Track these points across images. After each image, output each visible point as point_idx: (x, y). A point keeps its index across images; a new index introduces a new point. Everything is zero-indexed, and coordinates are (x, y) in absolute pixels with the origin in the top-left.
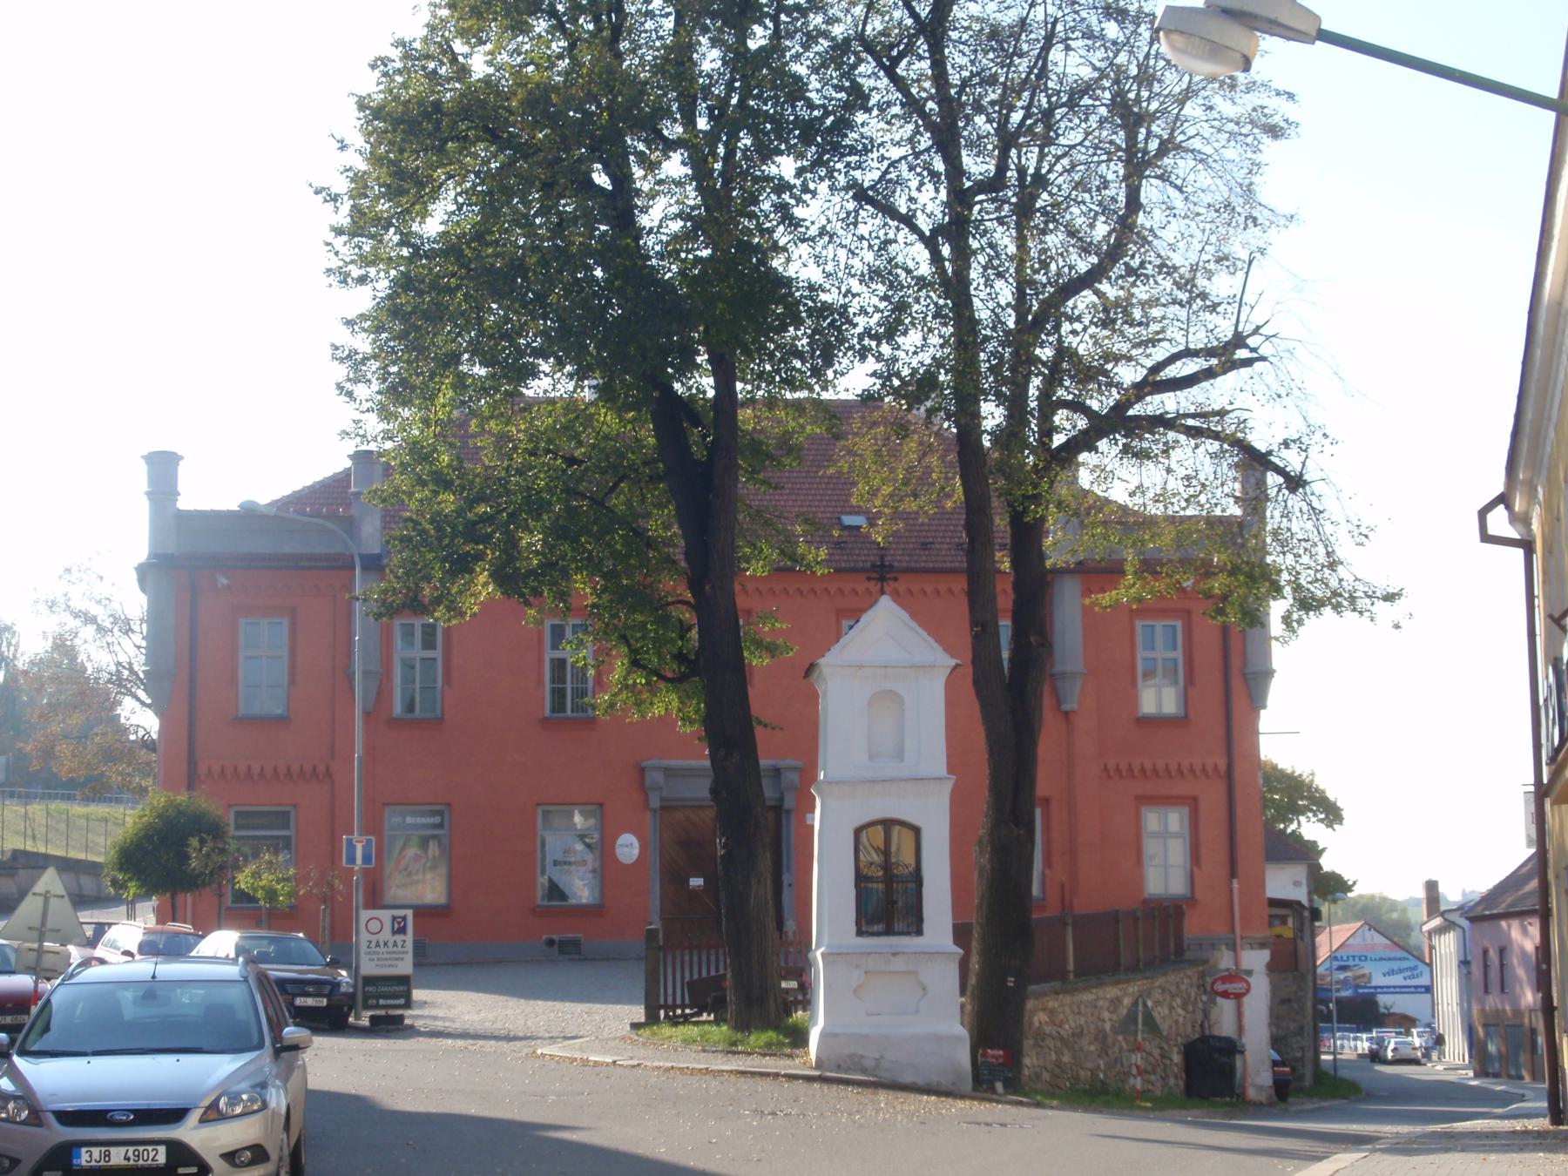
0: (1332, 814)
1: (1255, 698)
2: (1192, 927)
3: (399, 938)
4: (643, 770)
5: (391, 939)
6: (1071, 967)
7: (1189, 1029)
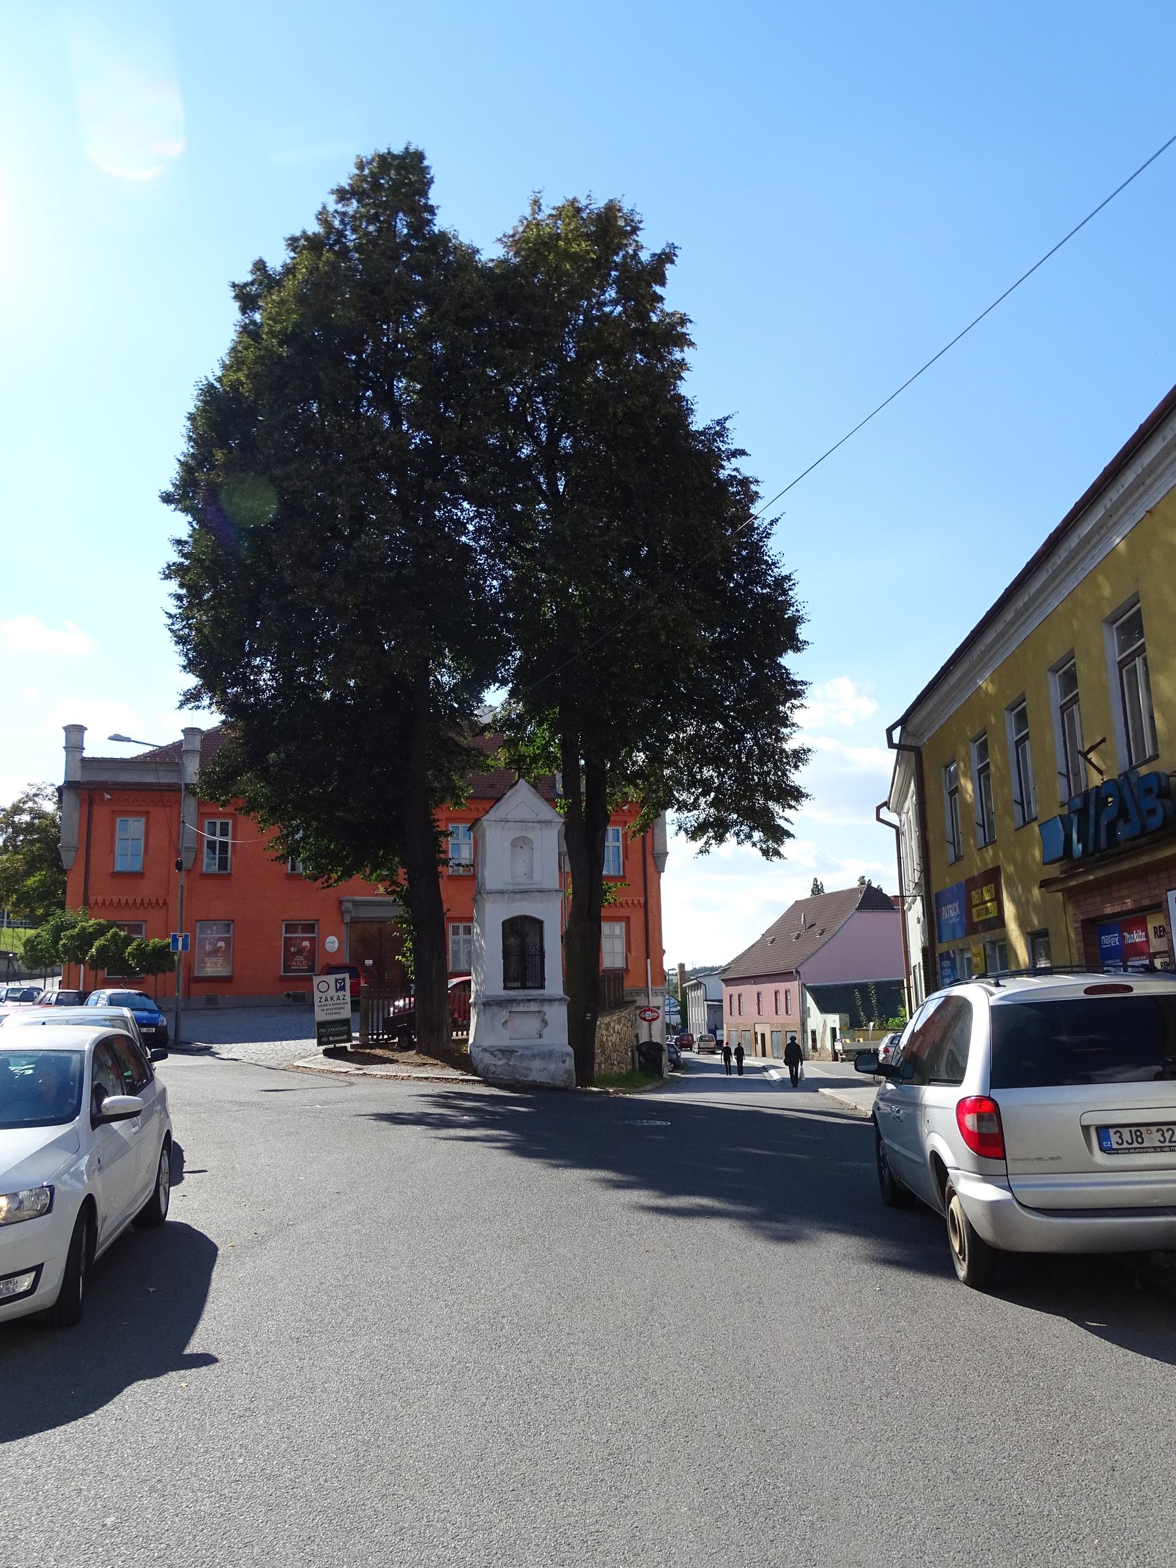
1: (659, 869)
2: (628, 984)
3: (341, 993)
4: (341, 902)
5: (335, 995)
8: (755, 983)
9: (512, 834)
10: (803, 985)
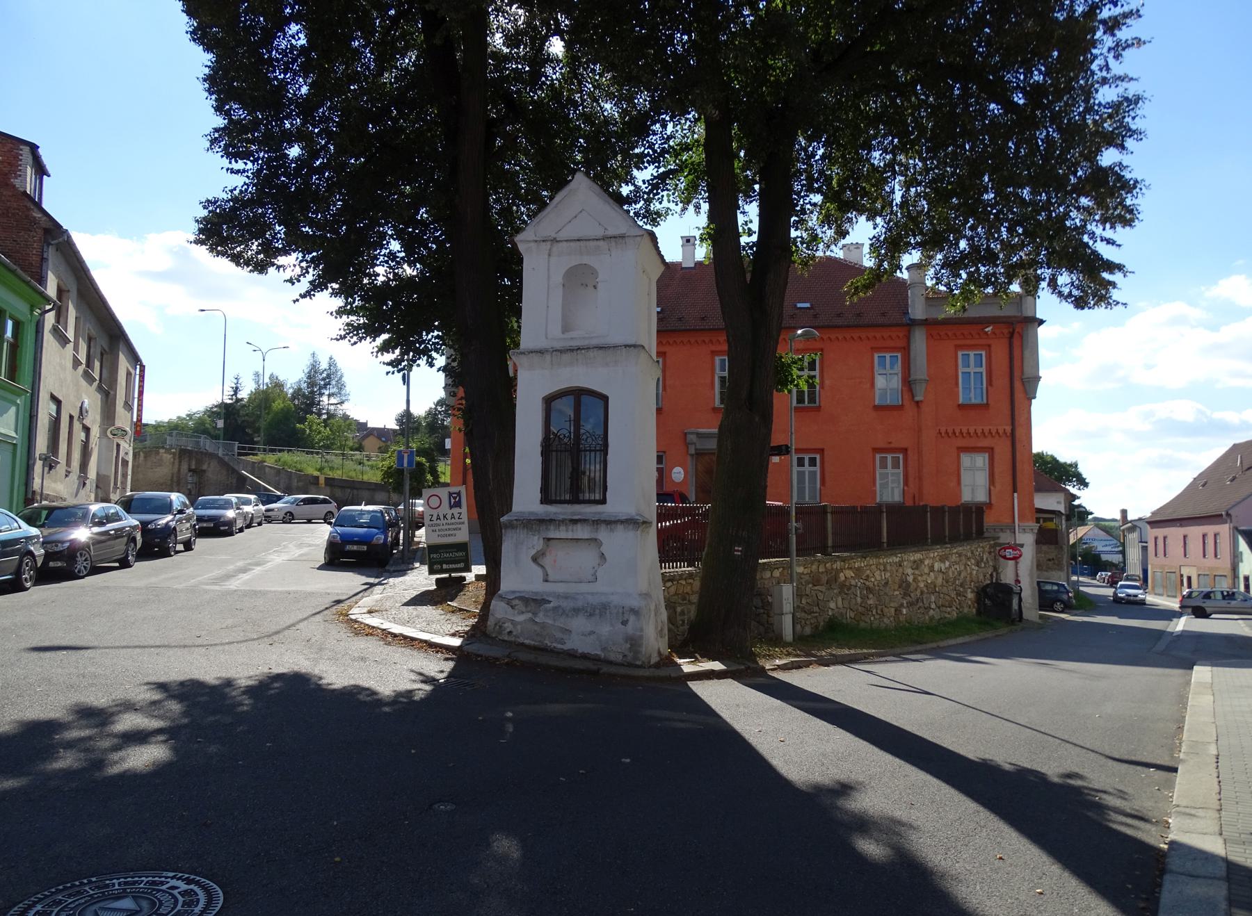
0: (1083, 483)
1: (1030, 395)
2: (989, 520)
3: (456, 511)
6: (830, 543)
7: (981, 577)
8: (1181, 526)
9: (563, 262)
10: (1236, 528)
